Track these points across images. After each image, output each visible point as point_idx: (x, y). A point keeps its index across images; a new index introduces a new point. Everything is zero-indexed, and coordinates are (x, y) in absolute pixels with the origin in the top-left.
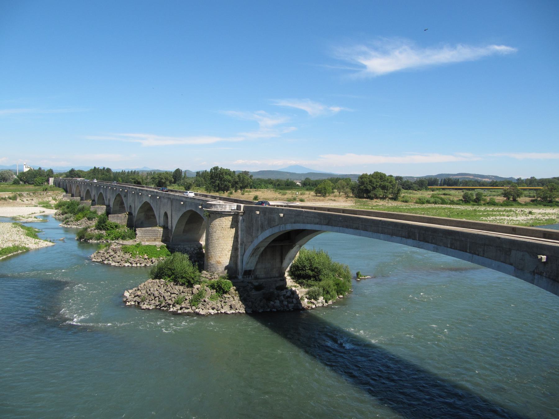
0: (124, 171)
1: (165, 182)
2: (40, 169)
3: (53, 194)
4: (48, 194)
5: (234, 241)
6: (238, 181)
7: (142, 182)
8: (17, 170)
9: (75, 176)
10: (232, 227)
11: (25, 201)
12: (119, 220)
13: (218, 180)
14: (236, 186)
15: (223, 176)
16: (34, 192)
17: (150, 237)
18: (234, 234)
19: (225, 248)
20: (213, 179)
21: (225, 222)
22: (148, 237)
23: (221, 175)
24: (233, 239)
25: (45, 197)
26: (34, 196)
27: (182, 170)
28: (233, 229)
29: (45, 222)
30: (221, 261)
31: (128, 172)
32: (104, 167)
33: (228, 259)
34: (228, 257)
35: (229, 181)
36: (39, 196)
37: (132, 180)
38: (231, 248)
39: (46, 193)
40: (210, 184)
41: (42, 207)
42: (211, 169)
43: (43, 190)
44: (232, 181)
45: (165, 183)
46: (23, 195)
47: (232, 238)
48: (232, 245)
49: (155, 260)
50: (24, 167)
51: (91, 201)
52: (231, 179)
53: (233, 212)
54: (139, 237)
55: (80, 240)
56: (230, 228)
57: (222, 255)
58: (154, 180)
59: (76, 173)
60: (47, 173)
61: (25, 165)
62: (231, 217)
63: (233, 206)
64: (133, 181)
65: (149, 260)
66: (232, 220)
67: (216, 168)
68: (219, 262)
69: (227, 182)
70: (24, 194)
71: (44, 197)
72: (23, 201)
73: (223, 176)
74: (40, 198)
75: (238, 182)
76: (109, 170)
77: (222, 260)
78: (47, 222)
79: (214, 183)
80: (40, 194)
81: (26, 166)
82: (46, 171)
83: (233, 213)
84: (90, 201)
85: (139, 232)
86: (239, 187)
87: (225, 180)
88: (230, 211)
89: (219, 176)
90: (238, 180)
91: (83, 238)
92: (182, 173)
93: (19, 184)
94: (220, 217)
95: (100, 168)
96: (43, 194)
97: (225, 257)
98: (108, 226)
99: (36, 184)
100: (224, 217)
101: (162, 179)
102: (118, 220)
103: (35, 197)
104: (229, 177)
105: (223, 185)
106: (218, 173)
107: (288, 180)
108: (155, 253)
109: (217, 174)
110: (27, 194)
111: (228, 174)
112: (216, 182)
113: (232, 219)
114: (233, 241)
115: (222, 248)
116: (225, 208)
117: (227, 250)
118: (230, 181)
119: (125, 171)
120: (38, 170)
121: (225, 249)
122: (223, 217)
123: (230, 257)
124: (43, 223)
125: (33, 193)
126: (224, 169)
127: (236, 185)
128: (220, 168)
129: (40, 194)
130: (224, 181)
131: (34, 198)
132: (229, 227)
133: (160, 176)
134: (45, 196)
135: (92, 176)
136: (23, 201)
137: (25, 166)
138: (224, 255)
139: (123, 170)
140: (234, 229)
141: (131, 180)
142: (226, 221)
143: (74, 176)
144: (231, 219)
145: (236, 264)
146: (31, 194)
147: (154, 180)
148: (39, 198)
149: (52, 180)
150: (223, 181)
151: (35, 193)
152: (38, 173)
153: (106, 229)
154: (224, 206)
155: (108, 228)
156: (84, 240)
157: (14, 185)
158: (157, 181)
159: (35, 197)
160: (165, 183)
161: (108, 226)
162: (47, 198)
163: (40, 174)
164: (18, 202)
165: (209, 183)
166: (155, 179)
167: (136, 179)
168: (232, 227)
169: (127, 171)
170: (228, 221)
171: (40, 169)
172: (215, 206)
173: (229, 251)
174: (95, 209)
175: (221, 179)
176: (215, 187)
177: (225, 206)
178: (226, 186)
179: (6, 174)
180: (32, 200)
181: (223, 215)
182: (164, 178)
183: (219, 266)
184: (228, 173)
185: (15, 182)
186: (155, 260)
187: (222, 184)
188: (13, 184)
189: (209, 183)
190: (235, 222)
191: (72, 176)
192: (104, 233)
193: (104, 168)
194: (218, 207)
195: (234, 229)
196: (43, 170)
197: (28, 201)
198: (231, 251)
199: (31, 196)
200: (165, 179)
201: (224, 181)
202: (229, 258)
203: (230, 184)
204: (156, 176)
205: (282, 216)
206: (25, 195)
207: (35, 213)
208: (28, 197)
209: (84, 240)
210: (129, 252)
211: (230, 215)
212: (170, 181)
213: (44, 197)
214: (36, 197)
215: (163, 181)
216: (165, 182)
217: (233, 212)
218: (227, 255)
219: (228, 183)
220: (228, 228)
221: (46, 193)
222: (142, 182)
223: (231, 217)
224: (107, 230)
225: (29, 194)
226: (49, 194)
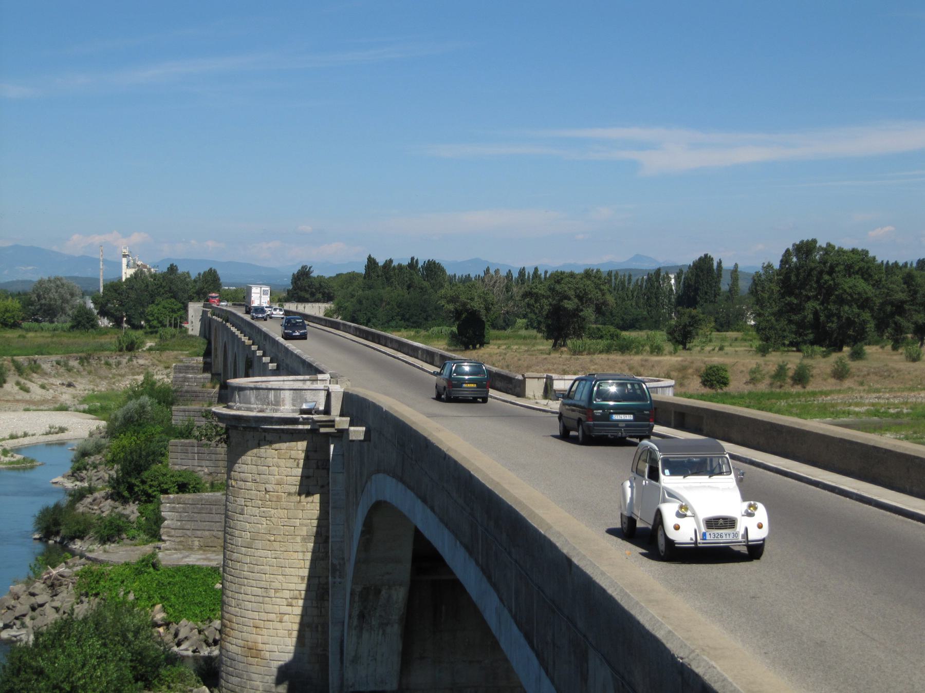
0: (492, 272)
1: (578, 309)
2: (172, 269)
3: (153, 365)
4: (135, 362)
5: (314, 552)
6: (903, 302)
7: (483, 312)
8: (98, 280)
9: (313, 294)
10: (305, 489)
11: (32, 389)
12: (208, 463)
13: (816, 298)
14: (896, 323)
15: (833, 279)
16: (83, 355)
17: (214, 533)
18: (315, 523)
19: (276, 585)
20: (791, 294)
21: (278, 467)
22: (207, 533)
23: (826, 277)
24: (311, 545)
25: (123, 376)
26: (81, 369)
27: (720, 263)
28: (310, 499)
29: (25, 469)
30: (260, 646)
31: (509, 275)
32: (412, 259)
33: (290, 635)
34: (289, 626)
35: (865, 303)
36: (104, 371)
37: (448, 302)
38: (303, 586)
39: (130, 360)
40: (779, 314)
41: (84, 412)
42: (787, 251)
43: (121, 350)
44: (878, 301)
45: (575, 313)
46: (39, 367)
47: (305, 540)
48: (305, 573)
49: (192, 629)
50: (120, 264)
51: (218, 386)
52: (870, 294)
53: (306, 421)
54: (173, 532)
55: (47, 542)
56: (300, 494)
57: (264, 616)
58: (532, 301)
59: (317, 285)
60: (199, 285)
61: (125, 256)
62: (302, 445)
63: (308, 395)
64: (451, 307)
65: (168, 629)
66: (307, 458)
67: (805, 249)
68: (253, 651)
69: (850, 306)
70: (45, 362)
71: (120, 375)
72: (27, 390)
73: (833, 279)
74: (106, 378)
75: (906, 307)
76: (433, 269)
77: (265, 639)
78: (32, 468)
79: (798, 309)
80: (107, 364)
81: (128, 262)
82: (194, 275)
83: (308, 427)
84: (214, 388)
85: (173, 510)
86: (912, 326)
87: (845, 296)
88: (297, 415)
89: (818, 282)
90: (901, 296)
91: (57, 533)
92: (723, 273)
93: (94, 326)
94: (259, 446)
95: (395, 263)
96: (119, 363)
97: (278, 625)
98: (151, 486)
99: (151, 327)
100: (275, 446)
101: (568, 298)
102: (204, 463)
103: (85, 373)
104: (862, 285)
105: (835, 319)
106: (812, 270)
107: (293, 274)
108: (198, 599)
109: (809, 274)
110: (58, 363)
111: (857, 273)
112: (804, 309)
113: (308, 452)
114: (309, 556)
115: (263, 584)
116: (278, 403)
117: (287, 594)
118: (867, 299)
119: (497, 271)
120: (164, 276)
121: (276, 590)
122: (271, 443)
123: (296, 627)
124: (13, 473)
125: (82, 360)
126: (841, 252)
127: (897, 318)
128: (824, 246)
129: (107, 364)
130: (841, 301)
131: (82, 376)
132: (295, 489)
133: (558, 287)
134: (123, 372)
135: (360, 292)
136: (27, 390)
137: (124, 261)
138: (272, 616)
139: (488, 270)
140: (317, 497)
141: (443, 302)
142: (282, 462)
143: (307, 296)
144: (302, 455)
145: (323, 660)
146: (74, 363)
147: (532, 301)
148: (100, 378)
149: (195, 311)
150: (835, 302)
151: (86, 358)
152: (164, 284)
153: (143, 498)
154: (272, 395)
155: (150, 491)
156: (58, 539)
157: (77, 333)
158: (546, 305)
159: (85, 373)
160: (575, 313)
161: (151, 486)
162: (130, 377)
163: (170, 290)
164: (9, 393)
165: (774, 314)
166: (537, 297)
167: (463, 298)
168: (305, 489)
169: (503, 273)
170: (291, 463)
171: (172, 269)
172: (241, 393)
173: (294, 602)
174: (185, 418)
175: (827, 293)
176: (801, 327)
177: (275, 396)
178: (850, 323)
179: (53, 295)
180: (70, 385)
181: (269, 437)
182: (571, 293)
183: (253, 669)
184: (857, 268)
185: (79, 323)
186: (192, 629)
187: (830, 316)
188: (72, 327)
189: (774, 314)
190: (318, 468)
191: (303, 294)
192: (133, 512)
193: (413, 264)
194: (253, 400)
195: (317, 497)
196: (183, 274)
197: (44, 391)
198: (301, 602)
199: (69, 370)
200: (577, 296)
201: (841, 301)
202: (295, 634)
203: (866, 315)
204: (542, 290)
205: (362, 438)
206: (46, 367)
207: (25, 435)
208: (58, 375)
209: (58, 539)
210: (97, 595)
211: (295, 436)
212: (597, 305)
213: (120, 375)
214: (90, 373)
215: (569, 305)
216: (578, 309)
217: (306, 421)
218: (286, 618)
219: (856, 310)
220: (290, 494)
221: (130, 360)
222: (483, 312)
223: (302, 445)
224: (146, 502)
225: (66, 365)
226: (141, 362)
